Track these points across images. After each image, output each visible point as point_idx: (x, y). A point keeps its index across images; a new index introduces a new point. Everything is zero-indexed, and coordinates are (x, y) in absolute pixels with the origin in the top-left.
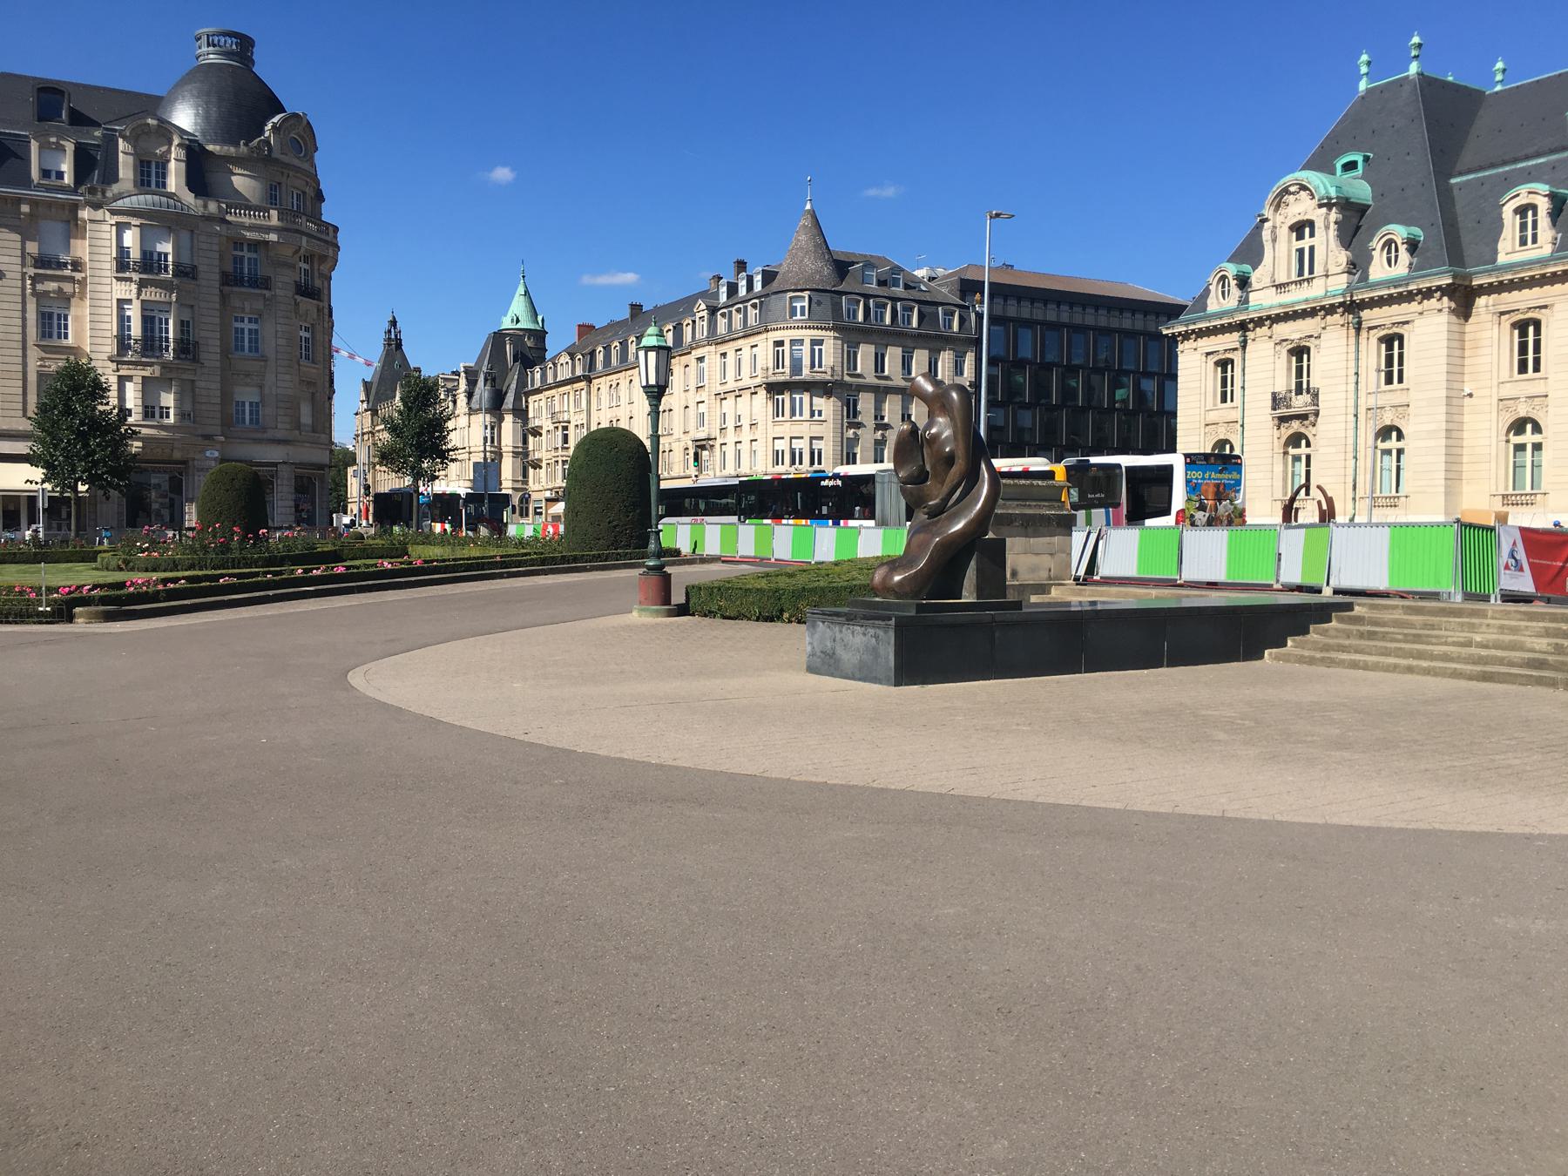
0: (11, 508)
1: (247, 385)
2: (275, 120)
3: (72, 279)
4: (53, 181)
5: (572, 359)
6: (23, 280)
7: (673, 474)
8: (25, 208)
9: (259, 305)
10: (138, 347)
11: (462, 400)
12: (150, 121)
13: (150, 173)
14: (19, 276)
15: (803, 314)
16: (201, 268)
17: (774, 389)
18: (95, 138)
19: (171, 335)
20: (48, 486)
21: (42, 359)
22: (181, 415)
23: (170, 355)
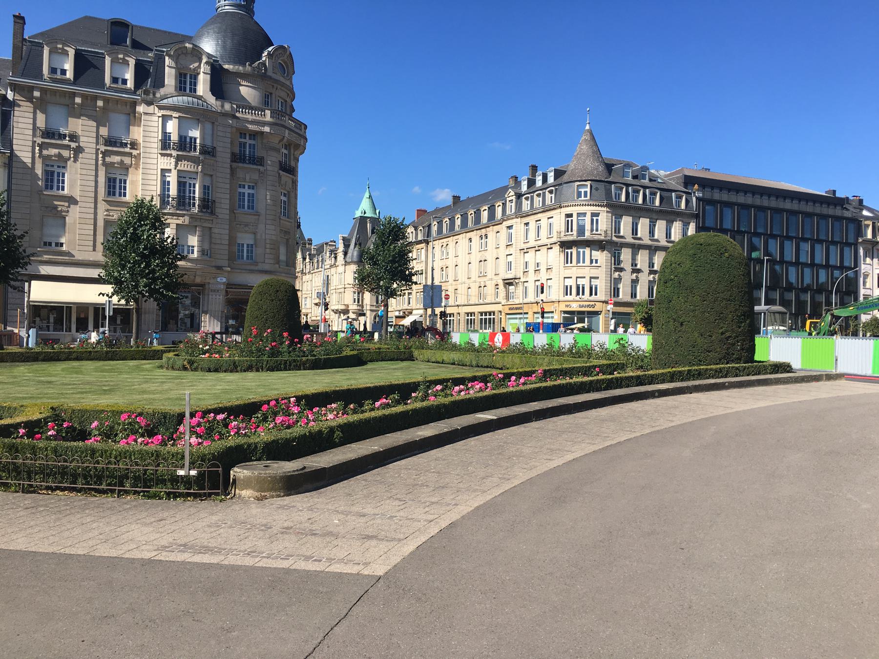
0: (82, 316)
1: (246, 232)
2: (270, 49)
3: (130, 155)
4: (120, 85)
5: (416, 229)
6: (97, 154)
7: (486, 301)
8: (100, 103)
9: (256, 176)
10: (174, 203)
11: (340, 256)
12: (187, 45)
13: (186, 83)
14: (94, 151)
15: (586, 196)
16: (218, 149)
17: (565, 245)
18: (149, 57)
19: (197, 195)
20: (115, 299)
21: (107, 210)
22: (202, 252)
23: (196, 210)
